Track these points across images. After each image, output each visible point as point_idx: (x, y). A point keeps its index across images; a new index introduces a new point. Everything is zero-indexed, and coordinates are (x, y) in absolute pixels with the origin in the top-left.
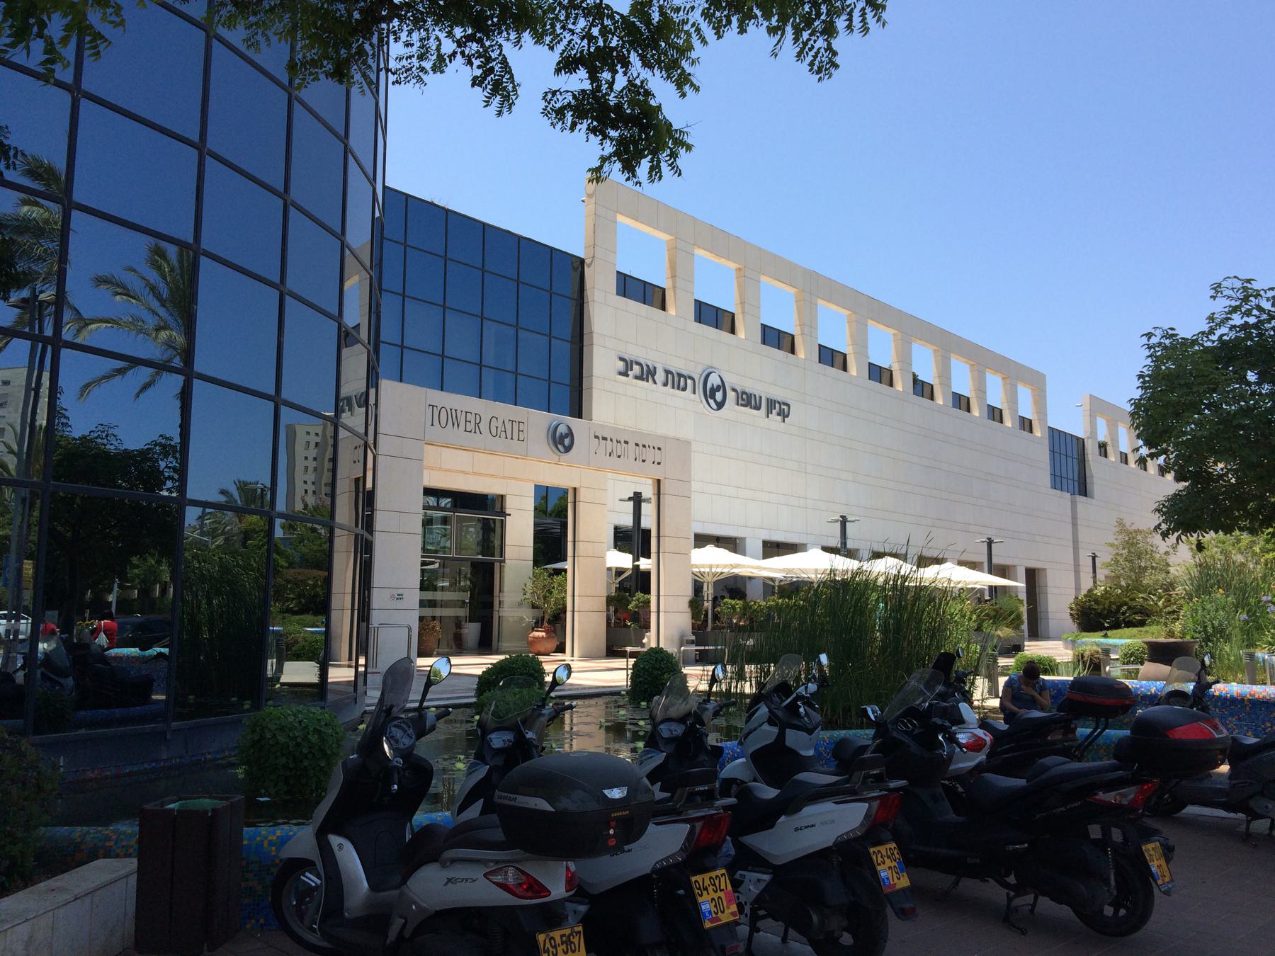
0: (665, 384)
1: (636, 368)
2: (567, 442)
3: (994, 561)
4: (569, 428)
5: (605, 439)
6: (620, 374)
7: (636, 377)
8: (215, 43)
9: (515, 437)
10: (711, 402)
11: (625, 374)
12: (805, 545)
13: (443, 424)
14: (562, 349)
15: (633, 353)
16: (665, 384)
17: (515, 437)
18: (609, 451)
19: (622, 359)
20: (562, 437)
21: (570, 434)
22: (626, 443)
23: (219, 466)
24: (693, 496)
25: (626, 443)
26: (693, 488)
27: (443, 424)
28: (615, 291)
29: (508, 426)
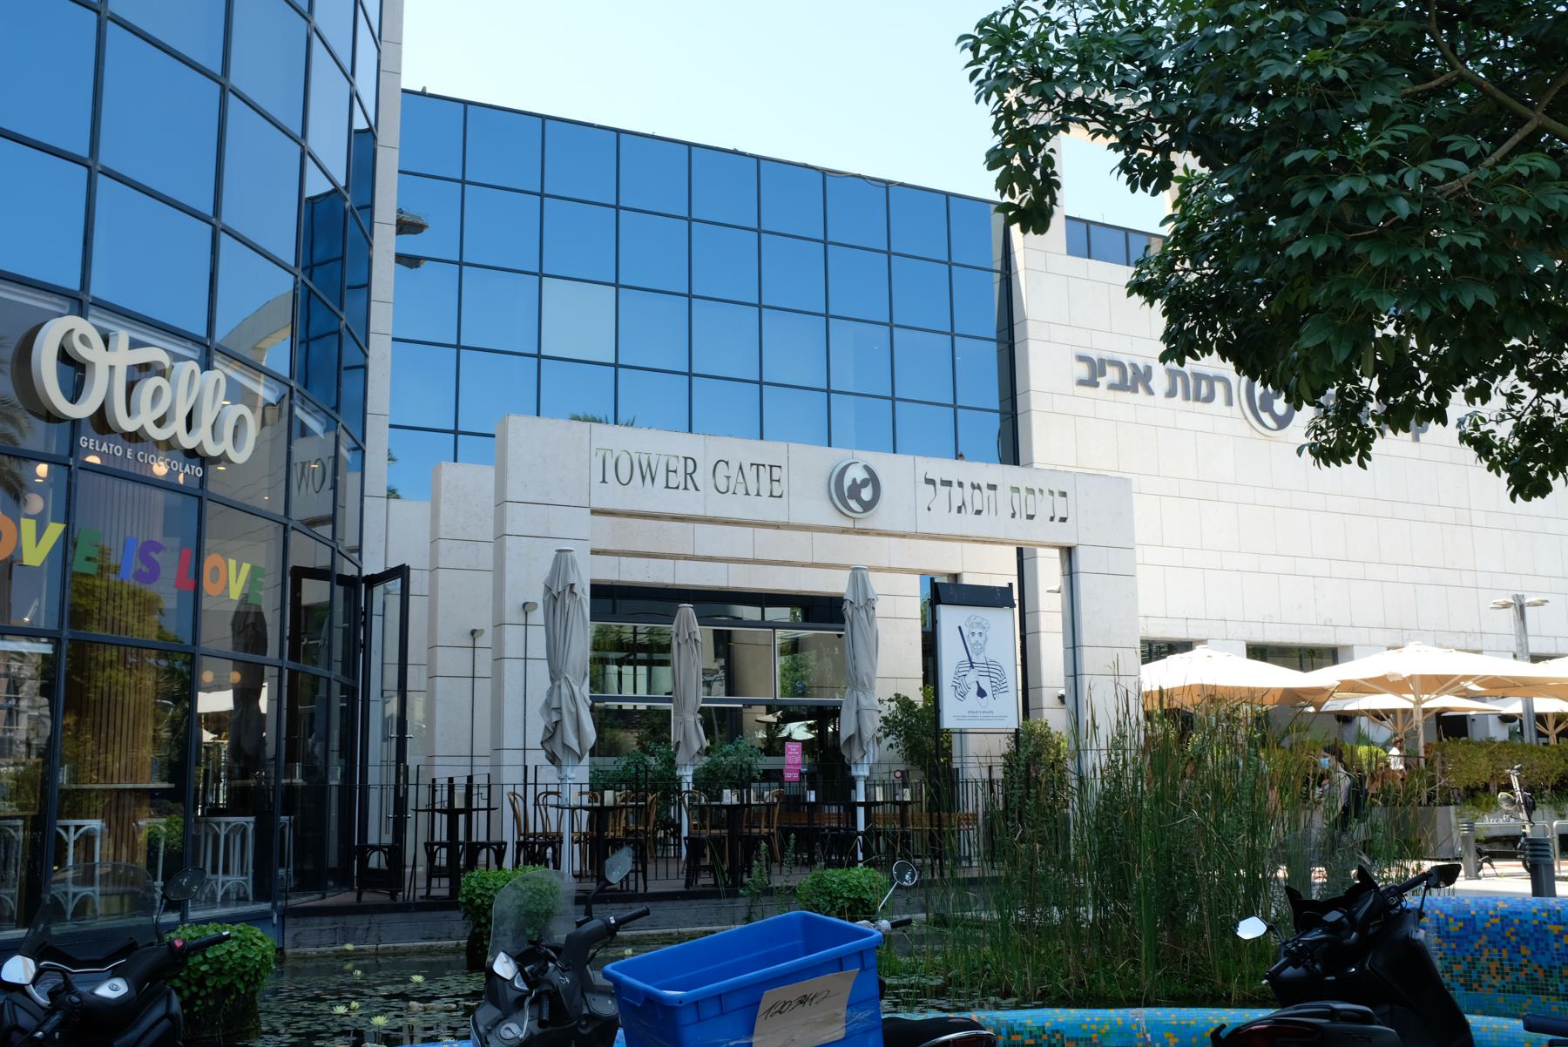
0: (1171, 393)
1: (1112, 374)
2: (866, 494)
3: (490, 472)
4: (867, 468)
5: (948, 483)
6: (1081, 383)
7: (1112, 387)
8: (232, 98)
9: (765, 492)
10: (1265, 417)
11: (1091, 382)
12: (1349, 648)
13: (624, 478)
14: (982, 358)
15: (1101, 347)
16: (1171, 393)
17: (765, 492)
18: (957, 503)
19: (1081, 358)
20: (855, 489)
21: (873, 479)
22: (993, 487)
23: (1002, 760)
24: (1140, 571)
25: (993, 487)
26: (1139, 559)
27: (624, 478)
28: (1064, 249)
29: (750, 474)
